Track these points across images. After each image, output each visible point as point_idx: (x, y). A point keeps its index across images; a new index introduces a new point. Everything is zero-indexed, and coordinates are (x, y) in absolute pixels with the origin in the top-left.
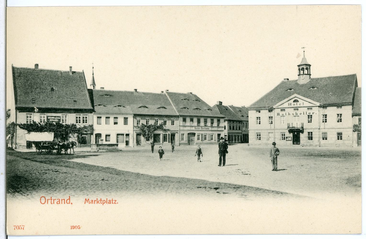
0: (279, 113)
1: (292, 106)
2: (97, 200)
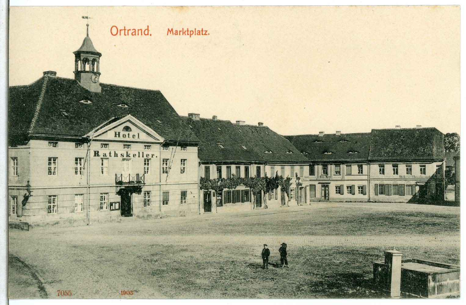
0: (98, 152)
1: (121, 138)
2: (183, 30)
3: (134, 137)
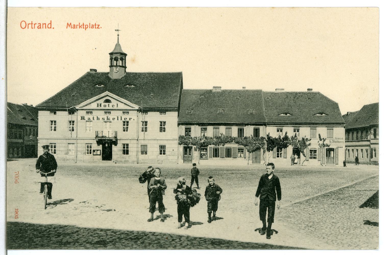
0: (84, 117)
1: (102, 107)
2: (79, 25)
3: (113, 106)
